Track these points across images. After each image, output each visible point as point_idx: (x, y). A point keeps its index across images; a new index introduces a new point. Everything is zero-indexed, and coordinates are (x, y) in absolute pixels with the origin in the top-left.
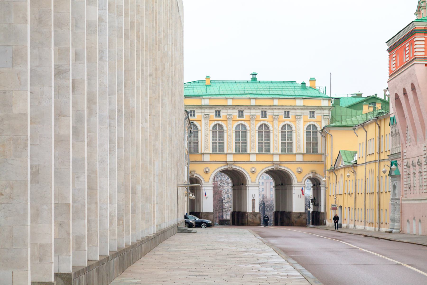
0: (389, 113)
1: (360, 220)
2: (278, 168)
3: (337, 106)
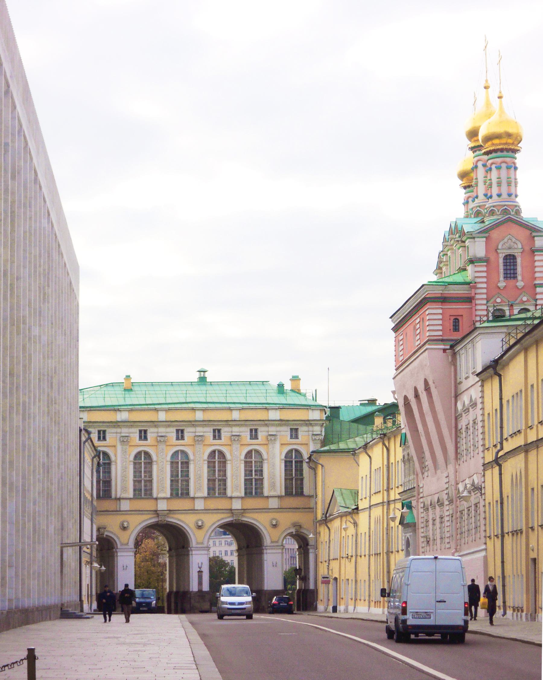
0: (400, 427)
1: (363, 598)
2: (239, 520)
3: (335, 420)
